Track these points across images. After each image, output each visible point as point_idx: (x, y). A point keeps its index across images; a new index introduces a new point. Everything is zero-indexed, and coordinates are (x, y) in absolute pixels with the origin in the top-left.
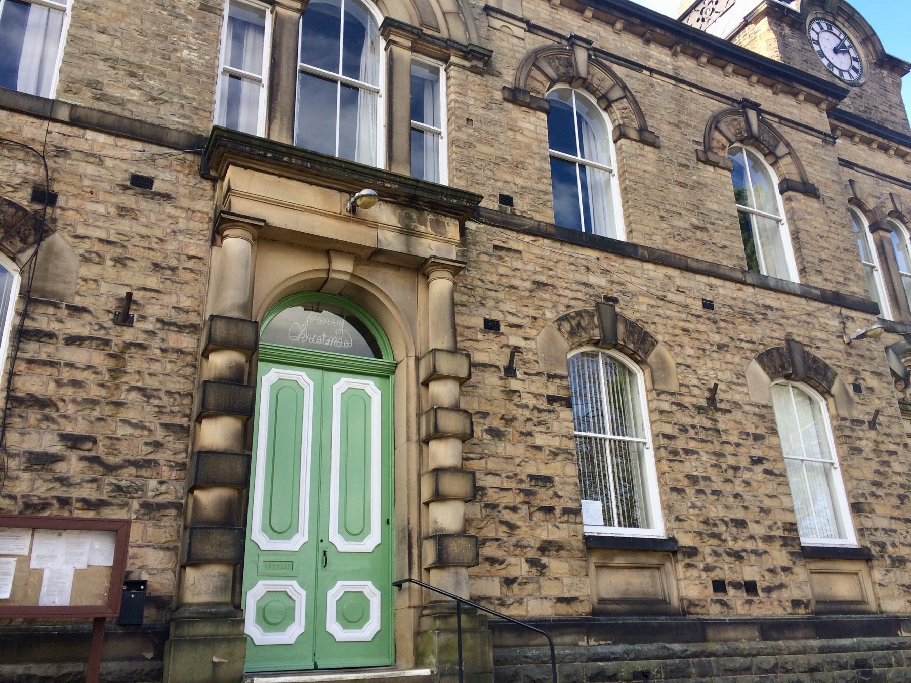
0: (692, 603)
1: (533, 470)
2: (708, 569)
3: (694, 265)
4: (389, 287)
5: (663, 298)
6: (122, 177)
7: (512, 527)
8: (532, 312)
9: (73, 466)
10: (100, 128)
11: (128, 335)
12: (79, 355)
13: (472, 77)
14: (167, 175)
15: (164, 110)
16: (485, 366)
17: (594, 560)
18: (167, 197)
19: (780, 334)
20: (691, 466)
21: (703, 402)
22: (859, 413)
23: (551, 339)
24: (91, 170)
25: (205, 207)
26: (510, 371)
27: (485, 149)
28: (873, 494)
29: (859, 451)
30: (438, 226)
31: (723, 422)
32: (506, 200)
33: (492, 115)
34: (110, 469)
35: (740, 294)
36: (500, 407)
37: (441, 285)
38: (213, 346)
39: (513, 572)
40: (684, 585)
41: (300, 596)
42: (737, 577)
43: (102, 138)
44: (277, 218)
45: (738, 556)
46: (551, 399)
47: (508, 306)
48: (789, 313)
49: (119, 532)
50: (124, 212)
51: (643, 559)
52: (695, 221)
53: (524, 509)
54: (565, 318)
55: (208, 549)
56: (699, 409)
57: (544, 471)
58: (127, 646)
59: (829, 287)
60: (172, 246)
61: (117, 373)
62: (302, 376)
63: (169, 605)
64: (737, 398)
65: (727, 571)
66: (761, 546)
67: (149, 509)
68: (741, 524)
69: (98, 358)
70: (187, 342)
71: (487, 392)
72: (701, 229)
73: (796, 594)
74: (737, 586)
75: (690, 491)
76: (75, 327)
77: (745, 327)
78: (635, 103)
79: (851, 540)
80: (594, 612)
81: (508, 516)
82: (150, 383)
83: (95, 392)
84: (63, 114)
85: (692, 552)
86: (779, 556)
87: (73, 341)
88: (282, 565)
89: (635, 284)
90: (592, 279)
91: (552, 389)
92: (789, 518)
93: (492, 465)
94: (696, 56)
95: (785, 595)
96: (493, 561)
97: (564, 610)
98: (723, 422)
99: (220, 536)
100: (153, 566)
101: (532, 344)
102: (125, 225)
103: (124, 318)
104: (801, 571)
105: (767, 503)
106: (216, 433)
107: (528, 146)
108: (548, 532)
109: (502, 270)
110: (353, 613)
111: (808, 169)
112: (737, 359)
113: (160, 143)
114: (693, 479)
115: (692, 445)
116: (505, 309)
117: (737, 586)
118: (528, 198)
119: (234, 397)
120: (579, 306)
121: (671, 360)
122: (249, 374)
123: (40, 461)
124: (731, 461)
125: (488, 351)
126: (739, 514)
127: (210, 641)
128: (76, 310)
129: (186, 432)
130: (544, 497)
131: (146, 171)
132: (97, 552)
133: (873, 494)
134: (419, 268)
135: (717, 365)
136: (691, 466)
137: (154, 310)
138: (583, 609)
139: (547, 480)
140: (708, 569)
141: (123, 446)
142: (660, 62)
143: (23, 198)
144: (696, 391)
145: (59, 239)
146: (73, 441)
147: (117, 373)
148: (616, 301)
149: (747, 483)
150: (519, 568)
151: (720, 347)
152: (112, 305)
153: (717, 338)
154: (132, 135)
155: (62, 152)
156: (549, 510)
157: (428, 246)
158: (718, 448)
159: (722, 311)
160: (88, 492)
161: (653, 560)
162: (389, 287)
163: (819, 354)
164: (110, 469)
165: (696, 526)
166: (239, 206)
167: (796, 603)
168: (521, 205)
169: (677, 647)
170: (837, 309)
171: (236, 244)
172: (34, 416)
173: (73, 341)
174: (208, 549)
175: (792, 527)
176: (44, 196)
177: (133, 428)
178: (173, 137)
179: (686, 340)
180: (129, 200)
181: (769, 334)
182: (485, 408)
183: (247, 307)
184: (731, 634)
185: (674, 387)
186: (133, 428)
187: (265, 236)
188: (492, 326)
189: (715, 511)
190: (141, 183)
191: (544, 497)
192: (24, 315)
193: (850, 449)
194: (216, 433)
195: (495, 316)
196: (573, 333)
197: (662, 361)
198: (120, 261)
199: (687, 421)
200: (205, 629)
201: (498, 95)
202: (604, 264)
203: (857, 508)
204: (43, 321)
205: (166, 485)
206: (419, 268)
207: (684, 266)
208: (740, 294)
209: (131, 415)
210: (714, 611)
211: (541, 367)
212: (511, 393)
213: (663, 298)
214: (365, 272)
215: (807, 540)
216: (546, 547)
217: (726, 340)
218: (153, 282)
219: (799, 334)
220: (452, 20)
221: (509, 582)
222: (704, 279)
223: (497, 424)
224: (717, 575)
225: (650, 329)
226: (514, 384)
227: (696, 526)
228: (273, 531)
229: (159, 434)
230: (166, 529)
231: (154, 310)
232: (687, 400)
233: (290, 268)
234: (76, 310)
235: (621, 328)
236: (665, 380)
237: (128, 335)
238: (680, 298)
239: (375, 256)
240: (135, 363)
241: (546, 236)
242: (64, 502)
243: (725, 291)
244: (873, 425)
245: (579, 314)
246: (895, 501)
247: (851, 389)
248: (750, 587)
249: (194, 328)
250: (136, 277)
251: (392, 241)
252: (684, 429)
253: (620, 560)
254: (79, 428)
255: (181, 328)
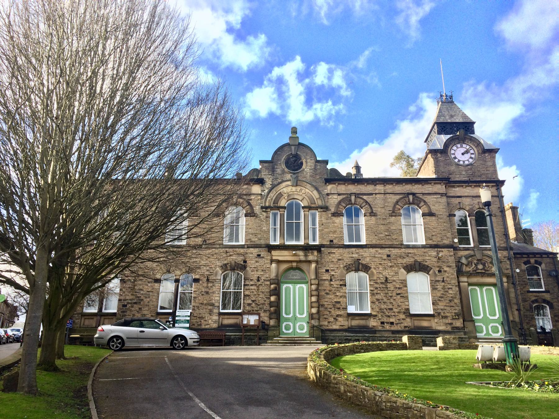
0: (374, 326)
1: (335, 300)
2: (379, 319)
3: (385, 246)
4: (304, 266)
5: (375, 257)
6: (256, 255)
7: (330, 312)
8: (337, 266)
9: (253, 305)
10: (252, 248)
11: (259, 283)
12: (253, 287)
13: (323, 213)
14: (263, 253)
15: (261, 241)
16: (325, 280)
17: (350, 318)
18: (263, 257)
19: (412, 260)
20: (378, 297)
21: (384, 281)
22: (439, 278)
23: (342, 272)
24: (251, 255)
25: (269, 258)
26: (331, 280)
27: (326, 230)
28: (439, 300)
29: (436, 289)
30: (312, 253)
31: (389, 285)
32: (331, 241)
33: (328, 221)
34: (259, 305)
35: (400, 251)
36: (329, 288)
37: (313, 265)
38: (271, 284)
39: (330, 320)
40: (373, 323)
41: (291, 325)
42: (387, 321)
43: (252, 249)
44: (280, 258)
45: (389, 316)
46: (341, 285)
47: (332, 266)
48: (417, 253)
49: (259, 314)
50: (257, 262)
51: (363, 317)
52: (387, 234)
53: (333, 309)
54: (346, 266)
55: (272, 317)
56: (382, 283)
57: (338, 300)
58: (263, 331)
59: (435, 243)
60: (265, 266)
61: (258, 290)
62: (290, 285)
63: (268, 325)
64: (394, 279)
65: (385, 319)
66: (396, 314)
67: (265, 311)
68: (391, 309)
69: (255, 287)
70: (268, 283)
71: (325, 285)
72: (388, 236)
73: (406, 325)
74: (387, 323)
75: (377, 303)
76: (252, 283)
77: (401, 260)
78: (370, 205)
79: (432, 312)
80: (349, 328)
81: (329, 310)
82: (263, 291)
83: (255, 293)
84: (246, 247)
85: (376, 316)
86: (402, 316)
87: (252, 285)
88: (287, 320)
89: (366, 255)
90: (354, 255)
91: (341, 283)
92: (407, 307)
93: (326, 300)
94: (392, 184)
95: (402, 325)
96: (326, 318)
97: (341, 327)
98: (389, 285)
99: (277, 314)
100: (266, 319)
101: (337, 274)
102: (257, 264)
103: (258, 280)
104: (408, 320)
105: (400, 304)
106: (273, 299)
107: (337, 226)
108: (339, 313)
109: (330, 258)
110: (302, 328)
111: (432, 207)
112: (396, 269)
113: (261, 248)
114: (378, 300)
115: (379, 292)
116: (331, 266)
117: (387, 323)
118: (337, 239)
119: (277, 292)
120: (349, 263)
121: (375, 271)
122: (213, 349)
123: (249, 305)
124: (390, 295)
125: (326, 276)
126: (391, 307)
127: (273, 330)
128: (251, 280)
129: (270, 298)
130: (338, 306)
131: (259, 253)
132: (256, 317)
133: (439, 300)
134: (310, 262)
135: (389, 271)
136: (378, 297)
137: (263, 278)
138: (346, 327)
139: (339, 302)
140: (379, 319)
141: (260, 301)
142: (379, 190)
143: (242, 263)
144: (382, 279)
145: (248, 269)
146: (253, 301)
147: (258, 290)
148: (360, 260)
149: (394, 300)
150: (332, 319)
151: (391, 266)
152: (256, 278)
153: (390, 264)
154: (257, 248)
155: (247, 253)
156: (339, 308)
157: (311, 258)
158: (386, 292)
159: (393, 257)
160: (256, 309)
161: (366, 318)
162: (304, 266)
163: (426, 264)
164: (259, 305)
165: (378, 310)
166: (274, 258)
167: (405, 327)
168: (335, 241)
169: (367, 335)
170: (436, 249)
171: (274, 265)
172: (248, 298)
173: (252, 285)
174: (272, 317)
175: (408, 309)
176: (245, 262)
177: (261, 298)
178: (263, 246)
179: (380, 266)
180: (257, 259)
181: (409, 260)
182: (325, 288)
183: (277, 276)
184: (383, 333)
185: (375, 278)
186: (261, 298)
187: (279, 262)
188: (327, 271)
189: (383, 307)
190: (259, 255)
191: (338, 306)
192: (244, 282)
193: (434, 288)
194: (273, 299)
195: (328, 268)
196: (347, 269)
197: (372, 273)
198: (257, 271)
199: (378, 286)
200: (273, 328)
201: (330, 215)
202: (357, 251)
203: (433, 304)
204: (247, 283)
205: (267, 307)
206: (310, 262)
207: (381, 247)
208: (400, 251)
209: (261, 296)
210: (380, 328)
211: (339, 278)
212: (331, 285)
213: (375, 257)
214: (299, 264)
215: (412, 312)
216: (337, 316)
217: (393, 264)
218: (262, 273)
219: (419, 259)
220: (318, 200)
221: (329, 322)
222: (388, 249)
223: (328, 292)
224: (382, 320)
225: (370, 265)
226: (332, 283)
227: (378, 310)
228: (286, 314)
229: (265, 299)
230: (268, 314)
231: (263, 278)
232: (379, 281)
233: (284, 266)
234: (251, 280)
235: (361, 266)
236: (373, 277)
237: (259, 283)
238: (380, 256)
239: (300, 261)
240: (261, 288)
241: (341, 248)
242: (253, 310)
243: (395, 251)
244: (443, 281)
245: (349, 265)
246: (448, 301)
247: (437, 272)
248: (392, 323)
249: (269, 280)
250: (260, 273)
251: (302, 258)
252: (376, 288)
253: (357, 318)
254: (254, 299)
255: (267, 281)
